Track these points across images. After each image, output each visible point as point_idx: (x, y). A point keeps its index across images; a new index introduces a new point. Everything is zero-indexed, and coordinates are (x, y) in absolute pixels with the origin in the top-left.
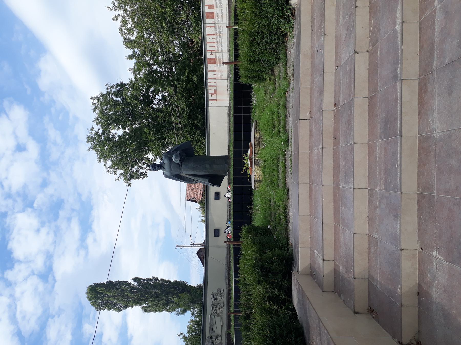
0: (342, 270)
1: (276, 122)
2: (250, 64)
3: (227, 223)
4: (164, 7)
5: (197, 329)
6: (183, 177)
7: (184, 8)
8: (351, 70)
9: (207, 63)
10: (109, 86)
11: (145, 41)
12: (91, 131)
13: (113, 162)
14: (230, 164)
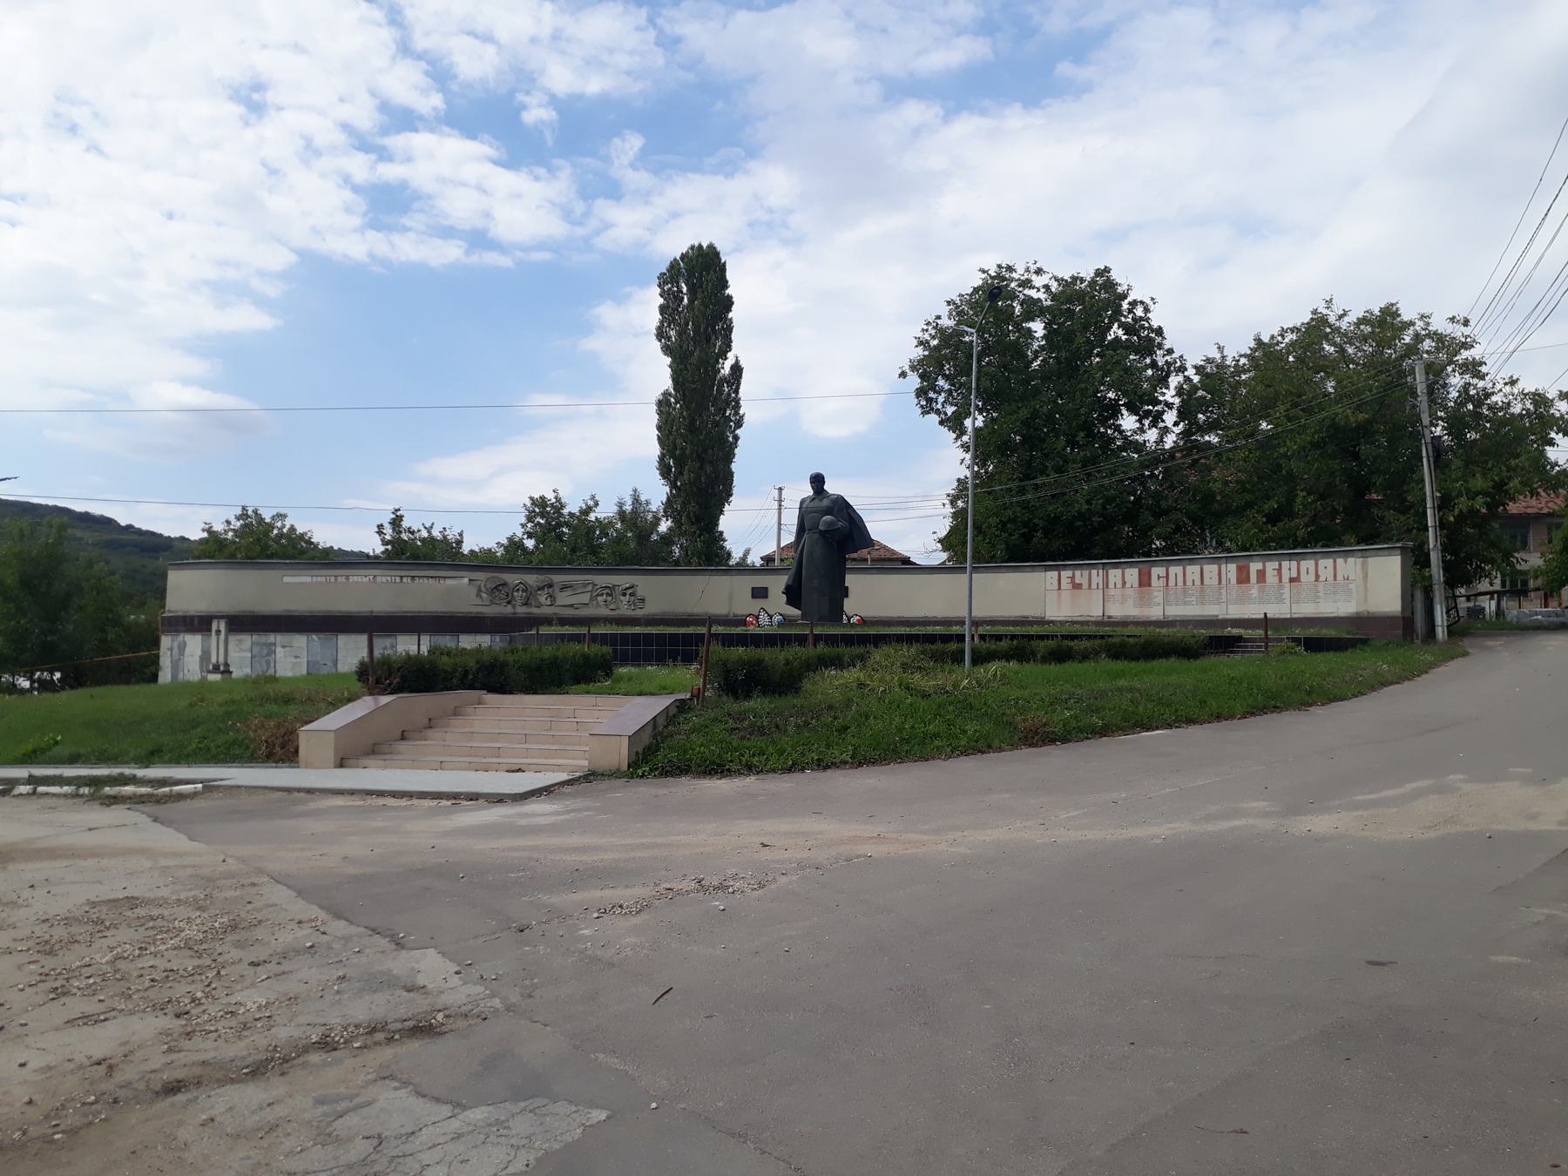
3: (781, 615)
9: (1141, 566)
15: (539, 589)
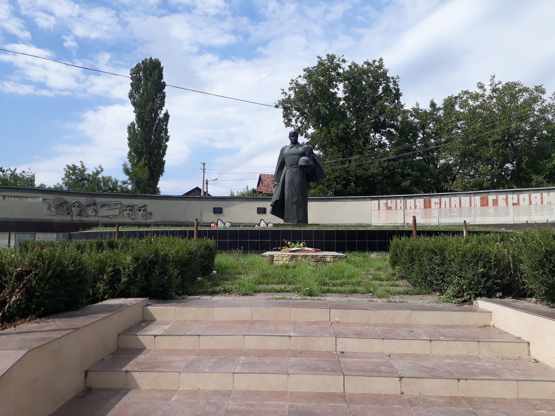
0: (141, 358)
1: (338, 281)
2: (409, 249)
3: (230, 223)
4: (495, 145)
5: (107, 188)
7: (494, 170)
8: (380, 372)
9: (425, 198)
10: (397, 80)
11: (452, 122)
12: (341, 60)
13: (304, 87)
14: (296, 225)
15: (87, 206)
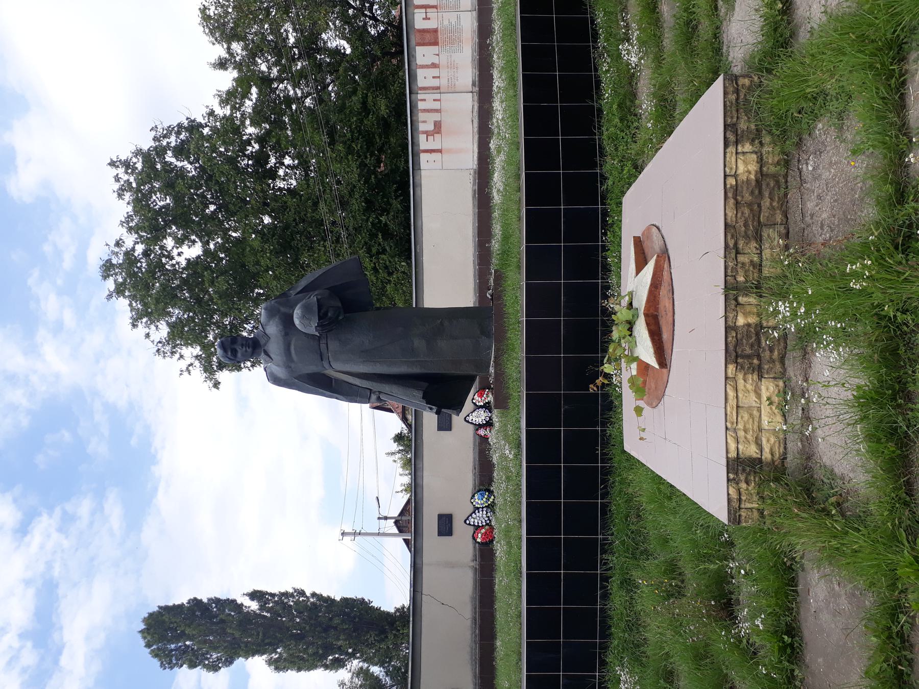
3: (473, 496)
6: (337, 380)
9: (413, 42)
12: (116, 250)
